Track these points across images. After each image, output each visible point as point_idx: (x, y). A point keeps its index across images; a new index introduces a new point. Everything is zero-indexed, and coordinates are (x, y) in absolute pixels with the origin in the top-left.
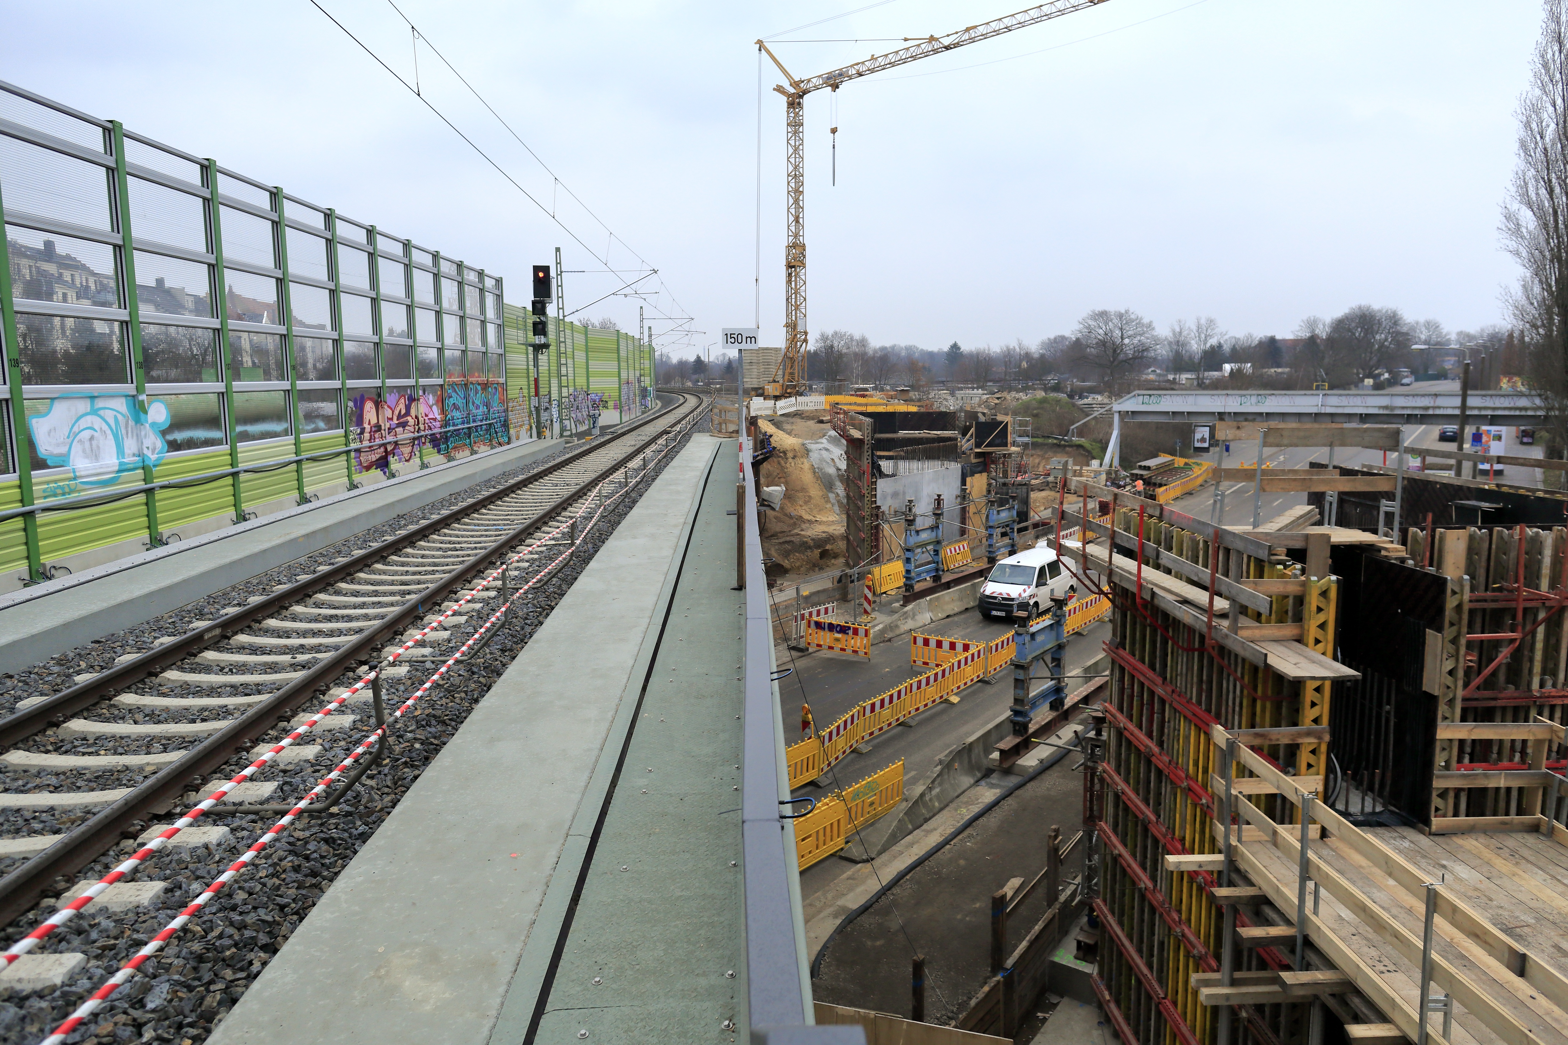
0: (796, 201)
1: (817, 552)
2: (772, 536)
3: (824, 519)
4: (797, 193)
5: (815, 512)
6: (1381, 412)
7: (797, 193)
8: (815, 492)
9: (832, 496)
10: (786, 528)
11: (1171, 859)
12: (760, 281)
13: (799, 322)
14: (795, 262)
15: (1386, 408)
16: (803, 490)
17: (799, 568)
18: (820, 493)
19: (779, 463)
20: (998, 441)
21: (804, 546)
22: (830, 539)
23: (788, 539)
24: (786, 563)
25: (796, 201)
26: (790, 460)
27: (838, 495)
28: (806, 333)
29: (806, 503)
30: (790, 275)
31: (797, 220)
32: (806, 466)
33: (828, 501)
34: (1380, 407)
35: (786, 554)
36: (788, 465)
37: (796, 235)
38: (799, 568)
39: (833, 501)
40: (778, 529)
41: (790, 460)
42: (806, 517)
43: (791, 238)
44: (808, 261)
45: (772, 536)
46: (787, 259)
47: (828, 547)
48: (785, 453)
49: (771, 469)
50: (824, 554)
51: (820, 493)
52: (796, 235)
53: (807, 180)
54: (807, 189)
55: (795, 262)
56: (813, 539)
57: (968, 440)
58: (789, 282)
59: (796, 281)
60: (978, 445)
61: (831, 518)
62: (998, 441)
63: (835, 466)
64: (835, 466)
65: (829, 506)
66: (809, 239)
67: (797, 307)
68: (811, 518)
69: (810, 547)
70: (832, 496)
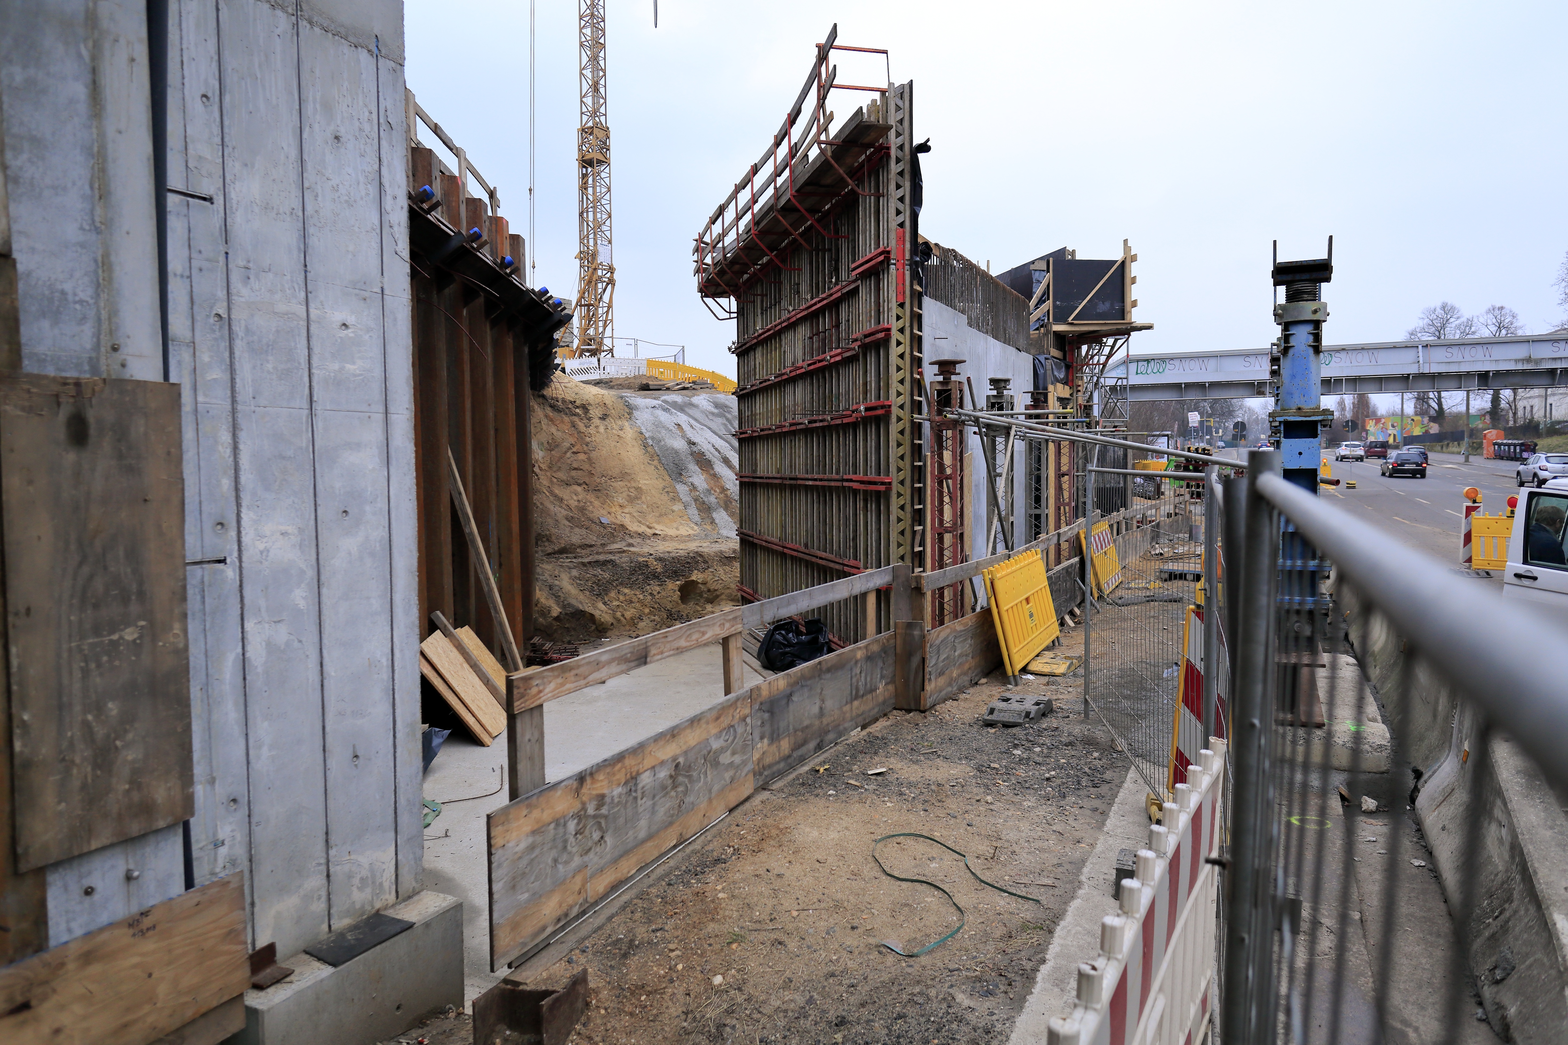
0: (594, 59)
1: (673, 586)
2: (563, 551)
3: (672, 532)
4: (594, 46)
5: (651, 519)
6: (1520, 367)
7: (594, 46)
8: (649, 480)
9: (682, 489)
10: (592, 539)
11: (438, 613)
12: (536, 191)
13: (600, 248)
14: (593, 159)
15: (1529, 360)
16: (624, 476)
17: (633, 622)
18: (660, 484)
19: (574, 425)
20: (1103, 307)
21: (642, 573)
22: (696, 560)
23: (601, 558)
24: (600, 611)
25: (594, 59)
26: (596, 421)
27: (694, 488)
28: (611, 269)
29: (631, 500)
30: (584, 176)
31: (595, 87)
32: (629, 433)
33: (676, 498)
34: (1517, 361)
35: (600, 590)
36: (592, 430)
37: (595, 113)
38: (633, 622)
39: (686, 498)
40: (576, 539)
41: (596, 421)
42: (633, 527)
43: (585, 118)
44: (614, 155)
45: (563, 551)
46: (580, 150)
47: (696, 576)
48: (585, 408)
49: (558, 435)
50: (688, 591)
51: (660, 484)
52: (595, 113)
53: (610, 26)
54: (610, 40)
55: (593, 159)
56: (660, 559)
57: (1041, 301)
58: (584, 187)
59: (594, 187)
60: (1061, 317)
61: (684, 531)
62: (1103, 307)
63: (684, 436)
64: (684, 436)
65: (678, 507)
66: (615, 118)
67: (598, 226)
68: (642, 529)
69: (655, 576)
70: (682, 489)
